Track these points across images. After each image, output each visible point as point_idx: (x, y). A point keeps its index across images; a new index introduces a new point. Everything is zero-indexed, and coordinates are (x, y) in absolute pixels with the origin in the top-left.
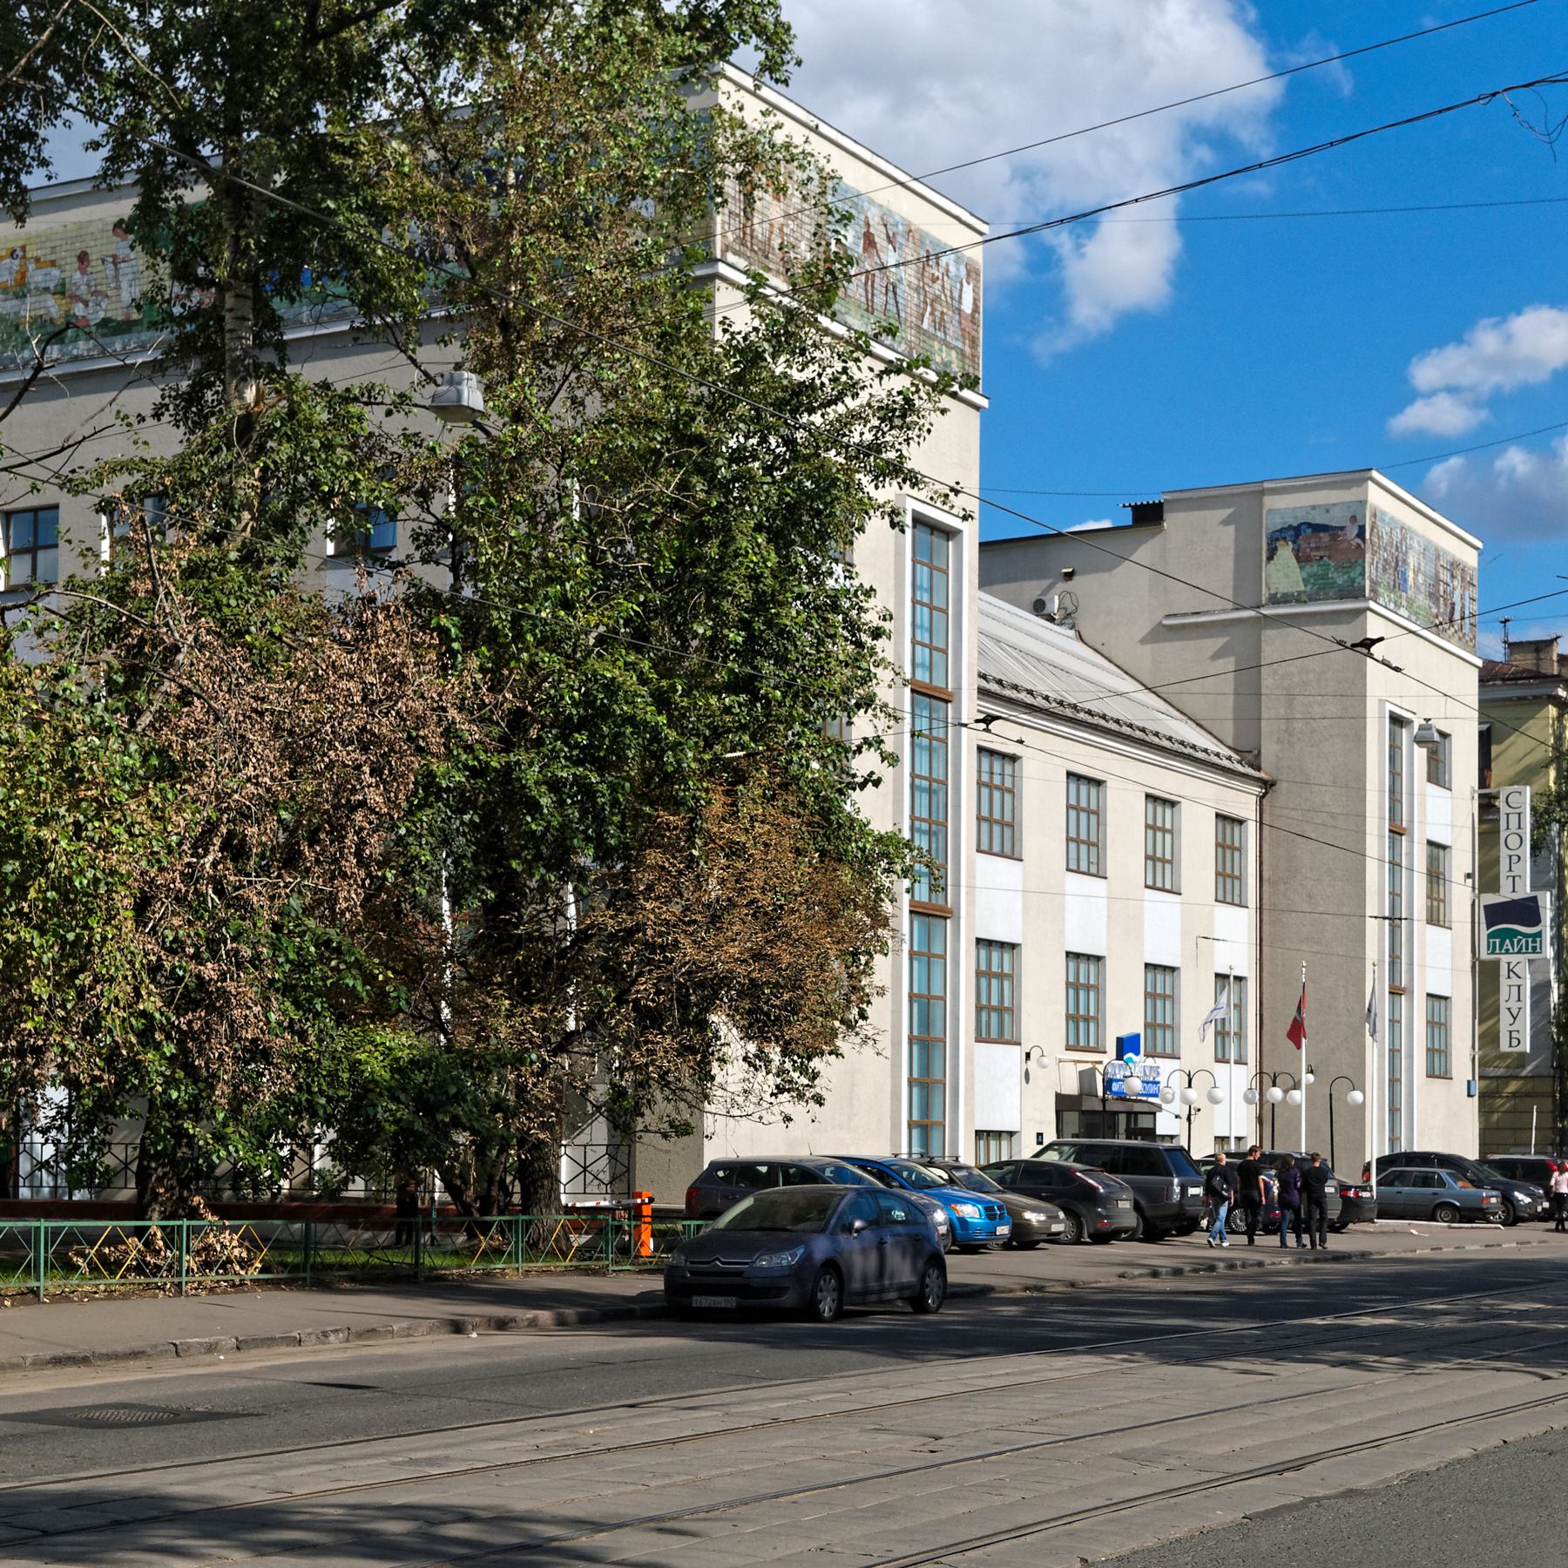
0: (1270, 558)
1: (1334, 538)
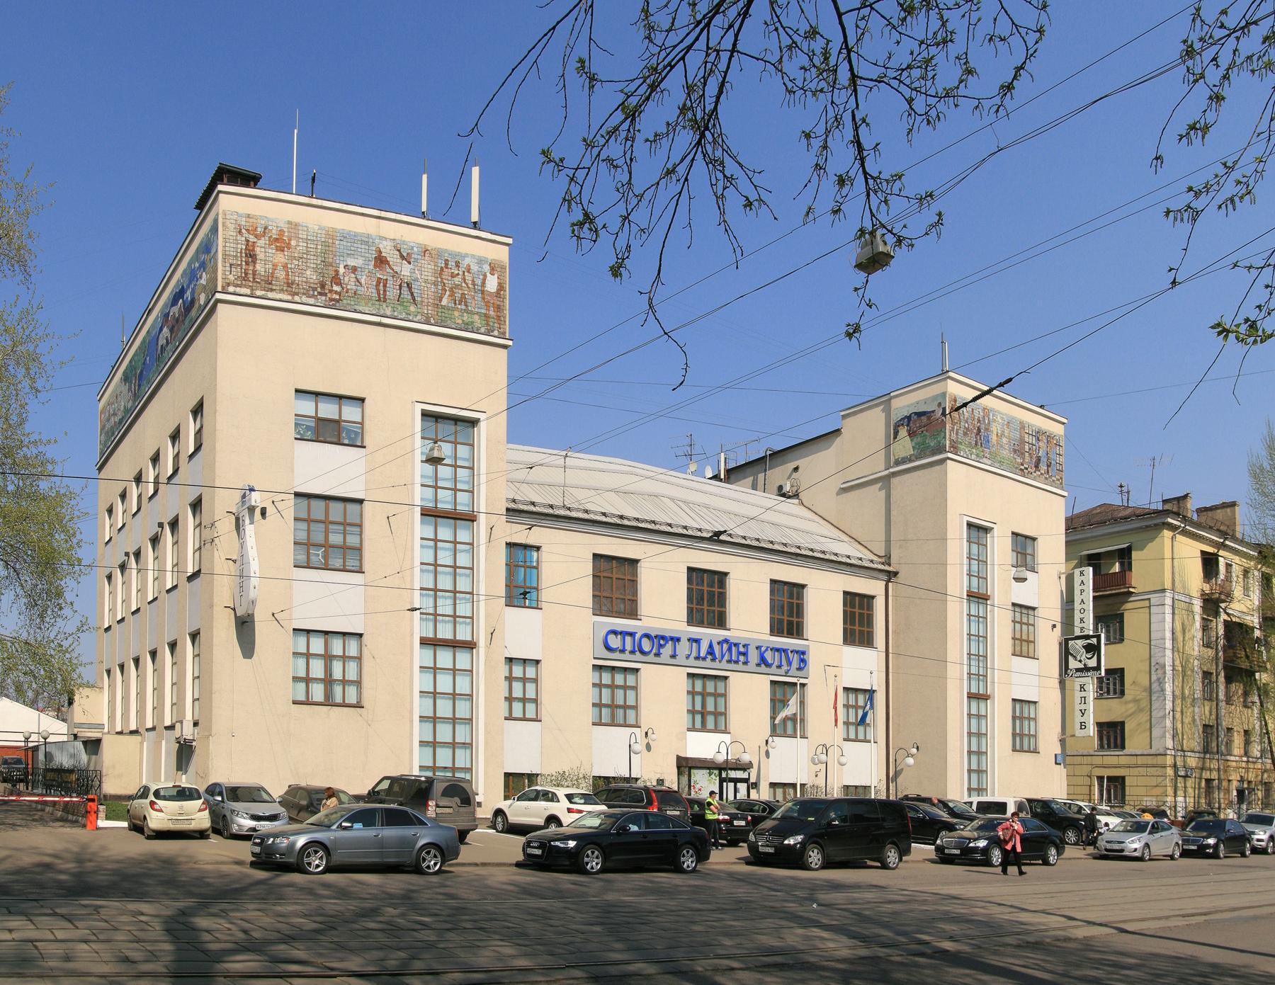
1: (929, 418)
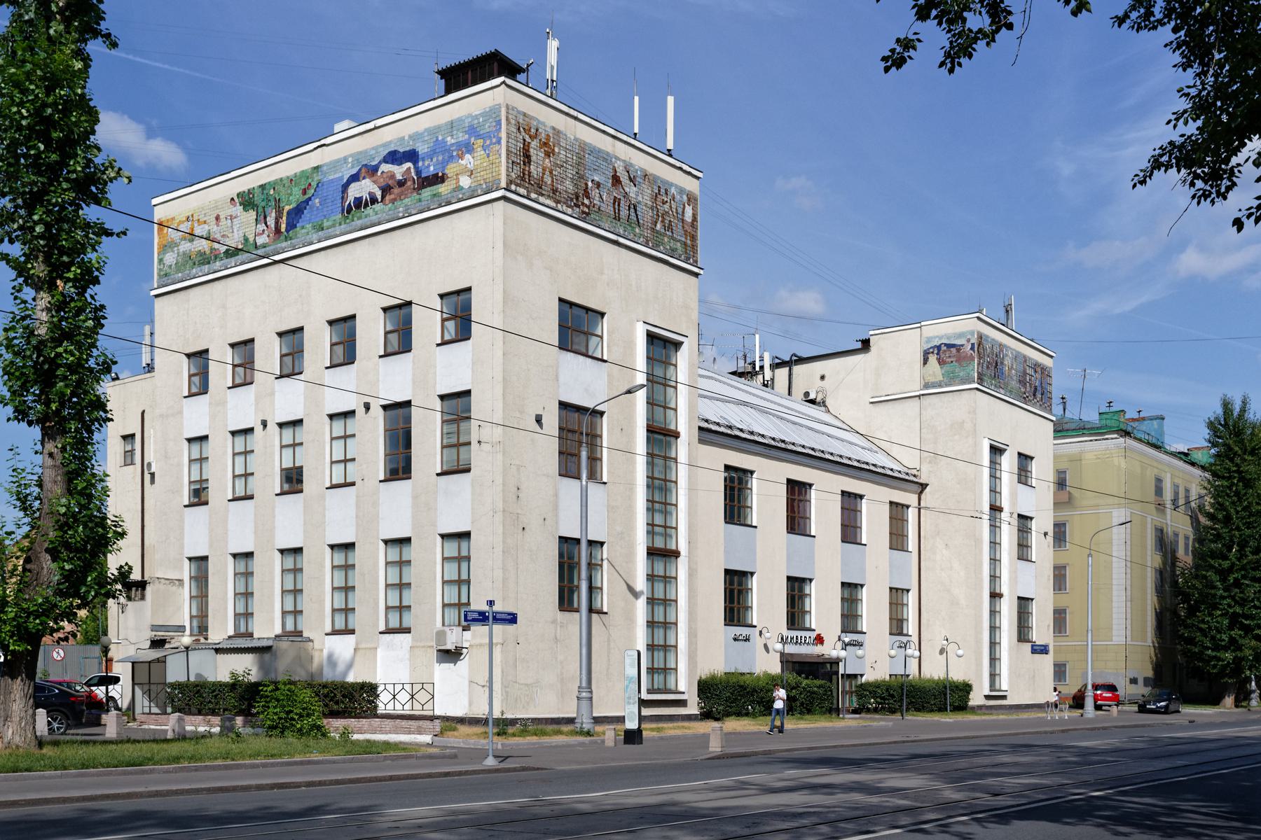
1: (958, 350)
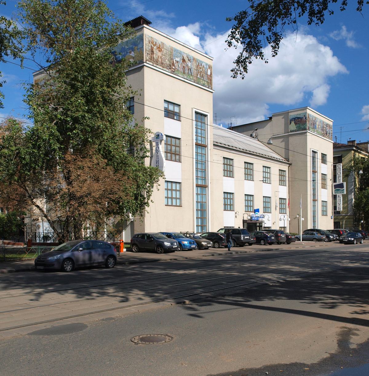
0: (290, 124)
1: (301, 120)
